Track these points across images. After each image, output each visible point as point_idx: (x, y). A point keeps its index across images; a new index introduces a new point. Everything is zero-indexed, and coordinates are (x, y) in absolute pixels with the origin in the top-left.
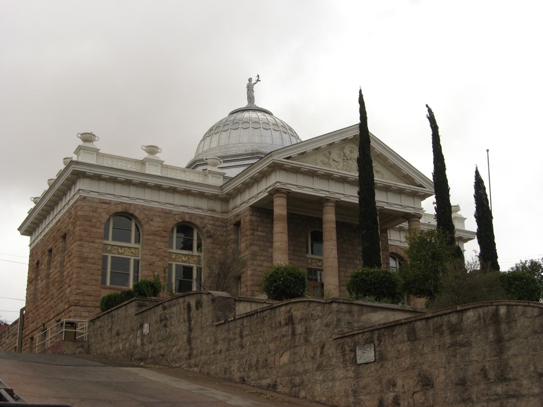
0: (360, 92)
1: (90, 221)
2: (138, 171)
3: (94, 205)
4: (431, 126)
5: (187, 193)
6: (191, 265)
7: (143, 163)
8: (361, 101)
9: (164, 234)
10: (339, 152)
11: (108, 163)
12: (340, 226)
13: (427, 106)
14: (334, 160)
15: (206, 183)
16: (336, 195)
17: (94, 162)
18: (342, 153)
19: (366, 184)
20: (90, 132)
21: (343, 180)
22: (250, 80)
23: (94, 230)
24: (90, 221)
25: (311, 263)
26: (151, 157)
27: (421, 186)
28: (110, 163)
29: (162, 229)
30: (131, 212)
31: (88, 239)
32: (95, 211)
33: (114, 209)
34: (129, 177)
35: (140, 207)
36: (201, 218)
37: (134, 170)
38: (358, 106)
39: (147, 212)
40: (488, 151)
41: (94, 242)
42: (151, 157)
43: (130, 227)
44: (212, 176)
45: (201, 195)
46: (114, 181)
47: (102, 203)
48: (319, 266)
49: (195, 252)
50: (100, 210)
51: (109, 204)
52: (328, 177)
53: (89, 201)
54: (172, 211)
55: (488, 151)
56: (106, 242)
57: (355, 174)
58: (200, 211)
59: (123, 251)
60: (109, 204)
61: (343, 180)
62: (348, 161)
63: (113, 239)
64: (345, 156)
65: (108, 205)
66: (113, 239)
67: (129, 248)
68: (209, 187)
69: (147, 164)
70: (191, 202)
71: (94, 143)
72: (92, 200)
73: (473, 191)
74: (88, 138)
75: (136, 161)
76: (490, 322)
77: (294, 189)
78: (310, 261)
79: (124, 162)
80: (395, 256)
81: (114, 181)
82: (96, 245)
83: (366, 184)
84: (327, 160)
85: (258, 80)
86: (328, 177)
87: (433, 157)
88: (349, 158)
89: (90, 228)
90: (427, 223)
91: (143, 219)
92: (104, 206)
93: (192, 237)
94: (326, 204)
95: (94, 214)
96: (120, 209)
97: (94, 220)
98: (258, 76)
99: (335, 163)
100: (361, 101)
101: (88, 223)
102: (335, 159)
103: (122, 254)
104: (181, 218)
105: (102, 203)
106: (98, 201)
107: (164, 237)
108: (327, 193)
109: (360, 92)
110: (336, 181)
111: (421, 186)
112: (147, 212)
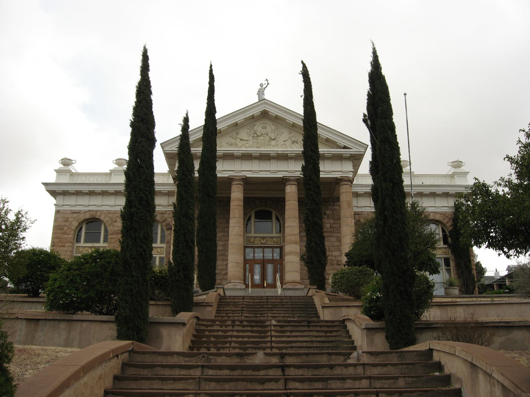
0: (211, 66)
1: (62, 229)
2: (448, 184)
3: (66, 216)
4: (304, 81)
7: (452, 176)
10: (249, 130)
11: (427, 182)
13: (302, 62)
14: (241, 140)
15: (453, 184)
16: (243, 173)
17: (67, 181)
18: (252, 131)
19: (311, 155)
20: (456, 160)
21: (283, 157)
22: (261, 85)
23: (65, 236)
24: (62, 229)
25: (253, 242)
26: (458, 170)
27: (345, 147)
28: (432, 181)
30: (97, 217)
31: (60, 244)
32: (66, 221)
33: (83, 217)
34: (92, 188)
35: (105, 212)
36: (162, 214)
37: (445, 184)
39: (111, 216)
40: (405, 94)
41: (64, 246)
42: (458, 170)
43: (100, 230)
44: (458, 177)
46: (91, 193)
47: (73, 213)
48: (262, 244)
50: (70, 219)
51: (79, 213)
53: (62, 213)
55: (405, 94)
56: (78, 245)
57: (299, 148)
58: (161, 207)
59: (265, 241)
60: (79, 213)
61: (283, 157)
62: (258, 138)
65: (78, 214)
66: (86, 241)
68: (362, 187)
69: (455, 176)
71: (462, 168)
74: (66, 162)
75: (445, 176)
77: (249, 175)
78: (252, 240)
79: (96, 176)
80: (5, 224)
81: (91, 193)
82: (66, 249)
83: (311, 155)
85: (268, 84)
87: (154, 110)
89: (61, 235)
90: (421, 183)
91: (107, 221)
92: (75, 215)
93: (100, 230)
94: (288, 183)
95: (66, 223)
96: (88, 216)
97: (65, 228)
98: (267, 80)
99: (242, 142)
101: (61, 231)
102: (242, 138)
105: (73, 213)
108: (340, 173)
109: (211, 66)
110: (295, 160)
111: (345, 147)
112: (111, 216)
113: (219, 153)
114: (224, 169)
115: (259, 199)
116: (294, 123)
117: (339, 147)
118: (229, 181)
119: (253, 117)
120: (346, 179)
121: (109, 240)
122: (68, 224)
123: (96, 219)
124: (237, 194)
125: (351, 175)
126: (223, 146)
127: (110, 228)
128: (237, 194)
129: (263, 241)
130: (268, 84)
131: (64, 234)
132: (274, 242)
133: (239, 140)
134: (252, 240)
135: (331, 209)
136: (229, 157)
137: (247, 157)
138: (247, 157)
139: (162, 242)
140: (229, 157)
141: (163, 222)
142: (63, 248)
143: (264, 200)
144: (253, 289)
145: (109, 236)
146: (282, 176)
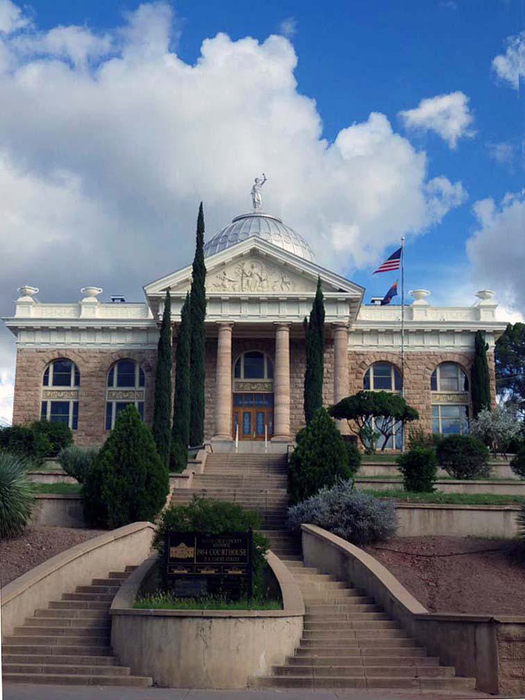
5: (105, 330)
6: (67, 400)
8: (201, 208)
9: (101, 373)
12: (292, 343)
27: (341, 291)
29: (98, 369)
38: (198, 211)
45: (120, 331)
49: (72, 387)
52: (254, 301)
54: (109, 350)
56: (111, 389)
59: (62, 394)
63: (245, 377)
64: (243, 272)
66: (245, 377)
67: (262, 383)
70: (100, 339)
72: (29, 351)
73: (198, 215)
76: (165, 513)
84: (220, 282)
85: (265, 180)
86: (254, 301)
88: (249, 275)
97: (31, 370)
100: (201, 208)
101: (25, 373)
103: (61, 397)
104: (119, 356)
106: (34, 350)
107: (101, 377)
111: (341, 291)
113: (207, 297)
114: (212, 314)
115: (250, 340)
116: (285, 263)
117: (335, 290)
118: (216, 327)
119: (241, 256)
120: (341, 324)
121: (81, 384)
122: (33, 364)
123: (65, 358)
124: (226, 341)
125: (346, 321)
126: (211, 288)
127: (81, 369)
128: (226, 341)
129: (253, 388)
130: (265, 180)
131: (28, 376)
132: (265, 388)
133: (227, 281)
134: (114, 394)
135: (328, 353)
136: (218, 301)
137: (236, 301)
138: (236, 301)
139: (142, 384)
140: (218, 301)
141: (142, 363)
142: (29, 392)
143: (254, 346)
144: (241, 442)
145: (81, 379)
146: (272, 321)
